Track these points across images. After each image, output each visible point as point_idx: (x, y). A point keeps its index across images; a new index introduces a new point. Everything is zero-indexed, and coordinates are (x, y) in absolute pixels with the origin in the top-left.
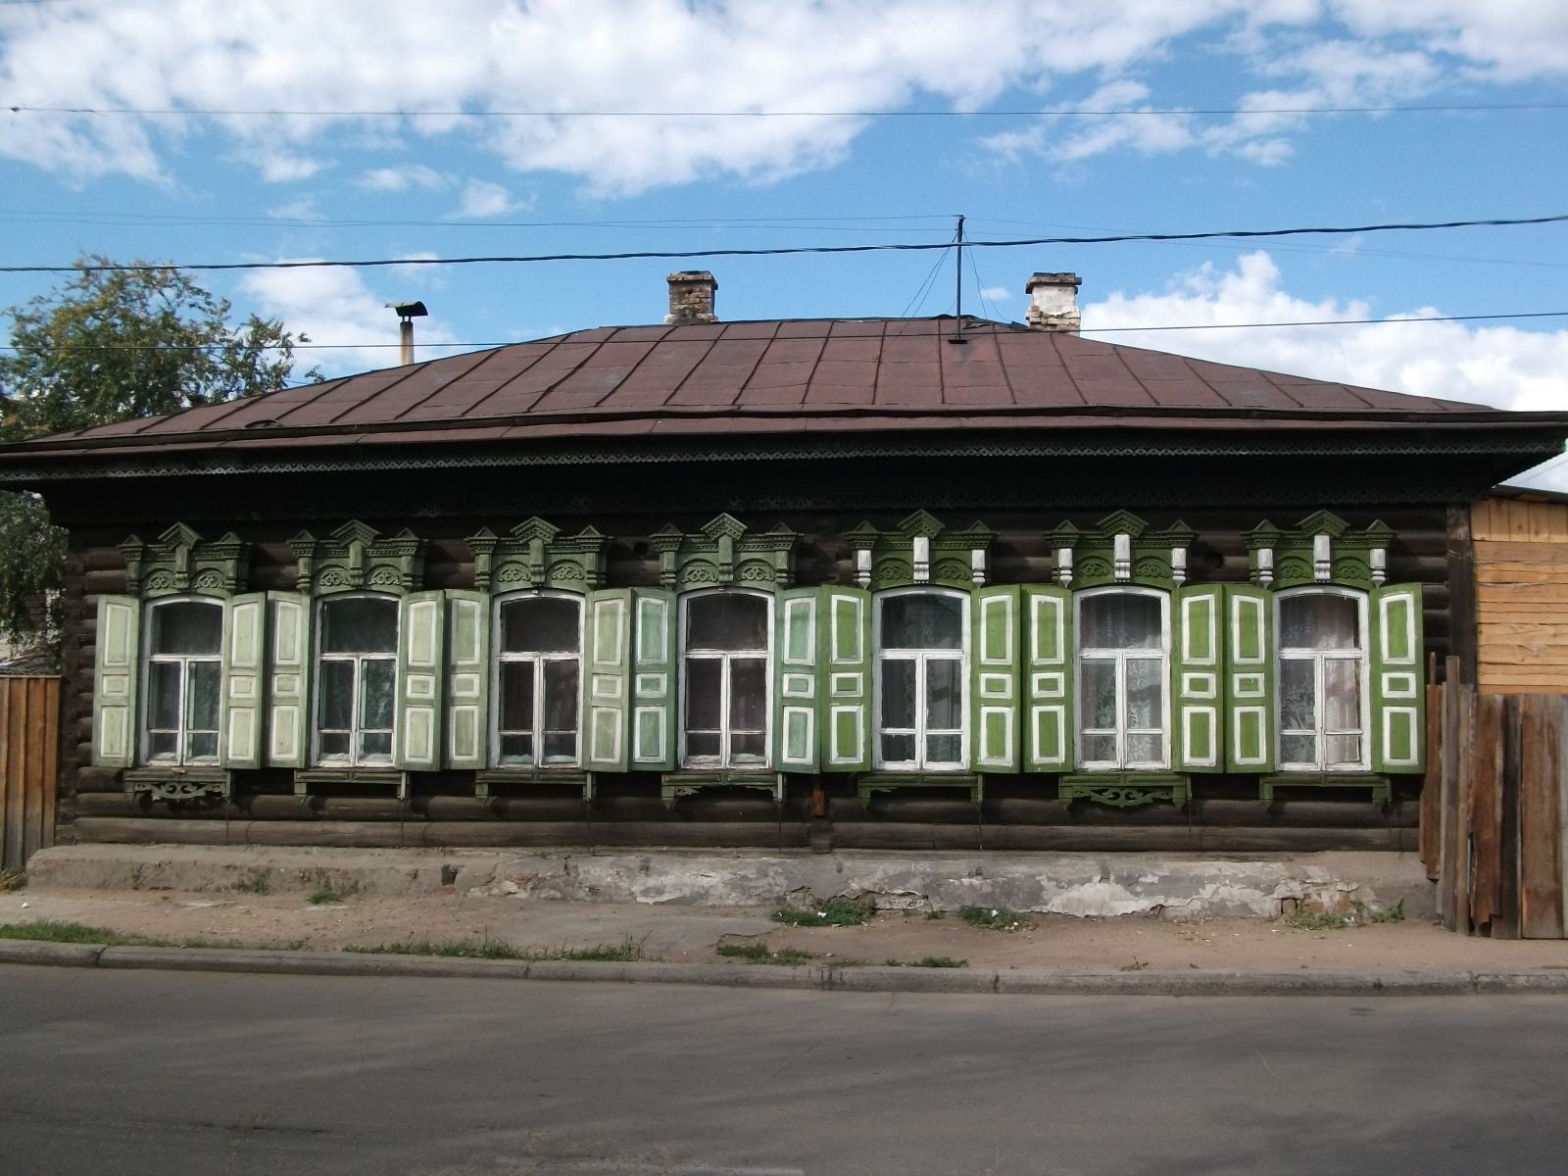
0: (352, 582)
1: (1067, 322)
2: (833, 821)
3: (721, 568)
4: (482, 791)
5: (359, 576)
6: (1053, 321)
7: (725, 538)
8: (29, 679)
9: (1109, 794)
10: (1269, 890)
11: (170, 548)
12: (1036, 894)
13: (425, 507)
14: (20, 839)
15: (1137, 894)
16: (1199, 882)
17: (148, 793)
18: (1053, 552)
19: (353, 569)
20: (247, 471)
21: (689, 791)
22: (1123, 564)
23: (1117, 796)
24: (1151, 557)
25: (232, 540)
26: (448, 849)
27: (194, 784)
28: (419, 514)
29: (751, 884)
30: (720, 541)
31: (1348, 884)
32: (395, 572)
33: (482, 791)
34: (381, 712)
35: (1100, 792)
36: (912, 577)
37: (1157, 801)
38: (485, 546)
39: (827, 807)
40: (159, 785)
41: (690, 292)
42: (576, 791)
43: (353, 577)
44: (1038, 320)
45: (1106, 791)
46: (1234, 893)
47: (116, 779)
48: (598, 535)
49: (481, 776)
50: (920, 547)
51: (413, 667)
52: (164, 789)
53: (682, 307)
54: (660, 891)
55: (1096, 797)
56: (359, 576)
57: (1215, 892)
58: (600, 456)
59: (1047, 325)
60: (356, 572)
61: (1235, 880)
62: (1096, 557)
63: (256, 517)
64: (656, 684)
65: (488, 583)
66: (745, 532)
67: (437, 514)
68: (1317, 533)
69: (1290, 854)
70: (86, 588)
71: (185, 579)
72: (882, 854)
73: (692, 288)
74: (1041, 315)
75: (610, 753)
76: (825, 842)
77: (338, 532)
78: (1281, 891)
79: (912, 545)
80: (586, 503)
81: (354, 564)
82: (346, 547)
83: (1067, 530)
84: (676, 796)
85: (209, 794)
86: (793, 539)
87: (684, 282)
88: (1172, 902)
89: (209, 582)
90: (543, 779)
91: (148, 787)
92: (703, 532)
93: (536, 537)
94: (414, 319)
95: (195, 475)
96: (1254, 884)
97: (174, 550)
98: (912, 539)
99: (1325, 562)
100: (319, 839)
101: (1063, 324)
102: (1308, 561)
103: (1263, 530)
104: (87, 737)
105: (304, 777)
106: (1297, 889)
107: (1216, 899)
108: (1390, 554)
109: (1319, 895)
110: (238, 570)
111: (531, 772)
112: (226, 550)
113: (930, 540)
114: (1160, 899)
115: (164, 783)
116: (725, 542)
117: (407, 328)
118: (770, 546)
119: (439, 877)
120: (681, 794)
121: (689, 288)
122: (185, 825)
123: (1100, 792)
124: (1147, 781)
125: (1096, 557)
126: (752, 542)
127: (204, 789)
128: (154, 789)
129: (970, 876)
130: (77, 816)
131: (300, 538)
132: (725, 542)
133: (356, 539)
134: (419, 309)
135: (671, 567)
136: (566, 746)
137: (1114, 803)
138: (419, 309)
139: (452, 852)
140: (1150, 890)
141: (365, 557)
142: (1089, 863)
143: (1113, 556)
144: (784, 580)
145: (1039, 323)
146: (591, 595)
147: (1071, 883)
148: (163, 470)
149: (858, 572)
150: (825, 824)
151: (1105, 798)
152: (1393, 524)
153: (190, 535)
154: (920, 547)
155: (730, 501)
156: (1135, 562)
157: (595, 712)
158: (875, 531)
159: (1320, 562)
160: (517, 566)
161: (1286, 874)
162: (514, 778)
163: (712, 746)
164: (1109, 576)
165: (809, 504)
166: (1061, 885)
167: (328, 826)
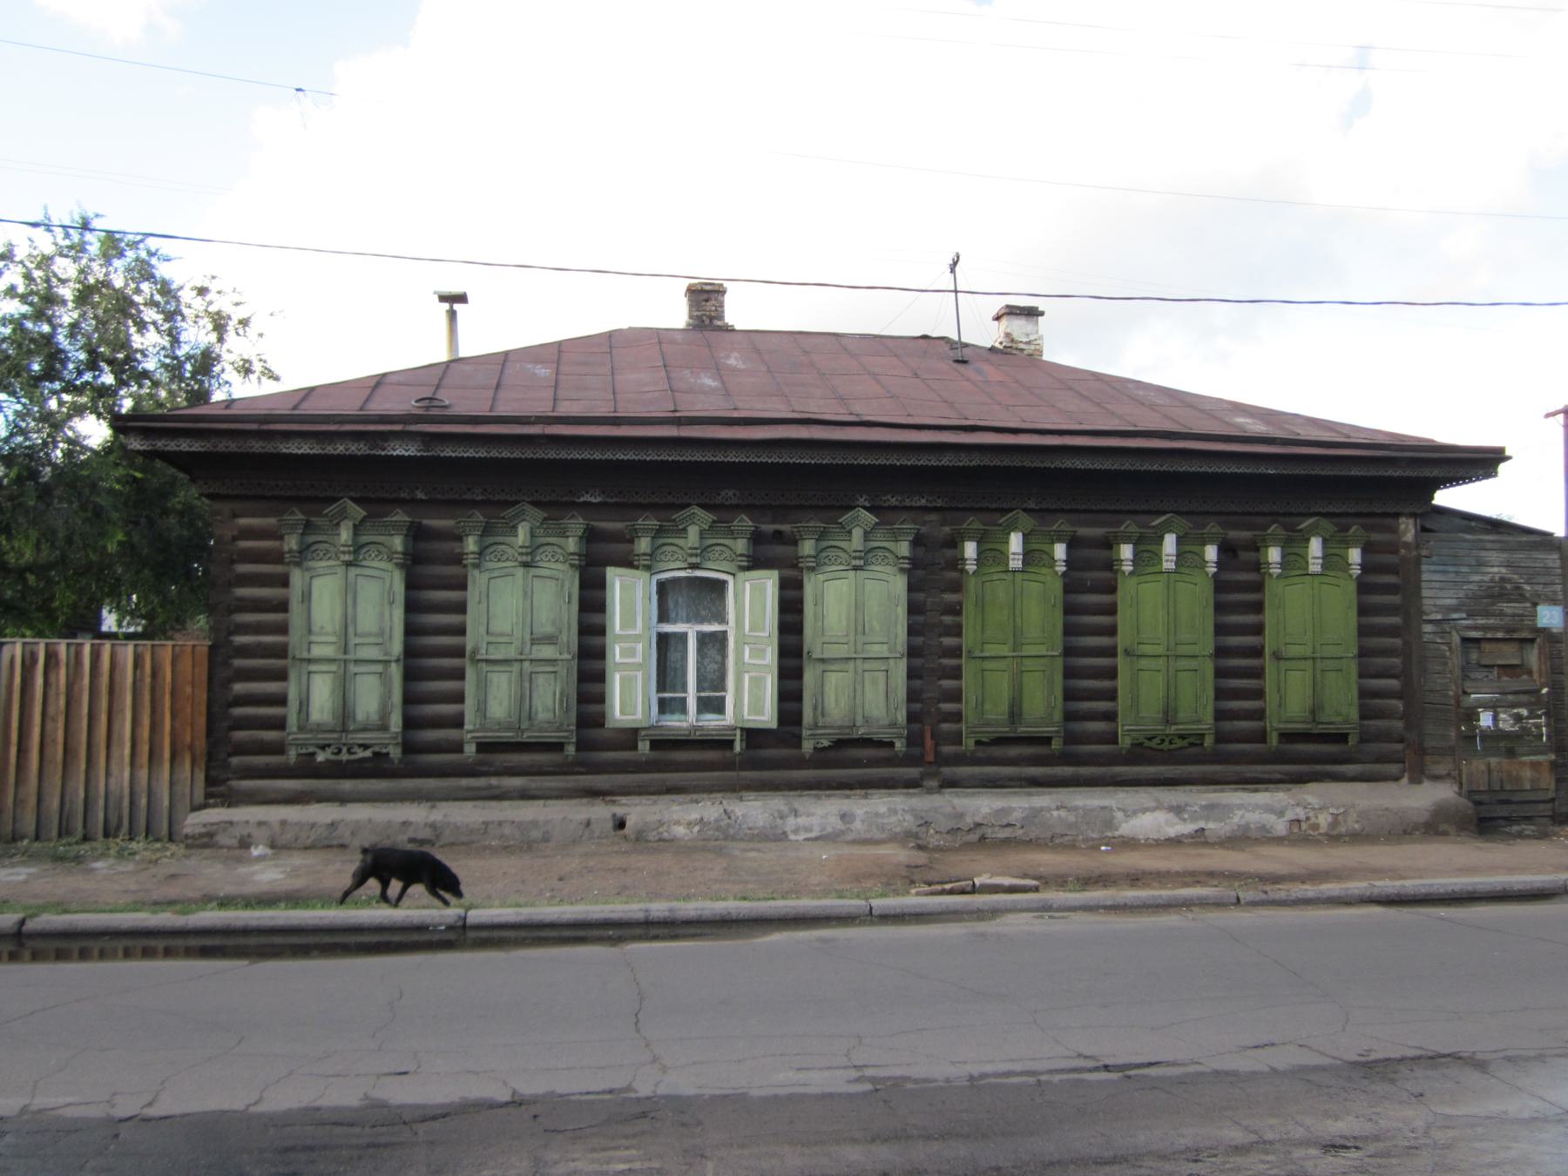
0: (520, 559)
1: (1033, 347)
2: (940, 766)
3: (690, 551)
4: (644, 747)
5: (527, 554)
6: (1021, 346)
7: (857, 529)
8: (194, 646)
9: (1157, 741)
10: (1281, 814)
11: (335, 522)
12: (1109, 824)
13: (587, 493)
14: (166, 803)
15: (1184, 820)
16: (1228, 809)
17: (313, 754)
18: (1115, 546)
19: (521, 547)
20: (430, 454)
21: (826, 743)
22: (1170, 558)
23: (1163, 741)
24: (548, 544)
25: (400, 517)
26: (608, 798)
27: (360, 746)
28: (582, 499)
29: (885, 821)
30: (853, 531)
31: (1338, 808)
32: (559, 551)
33: (644, 747)
34: (713, 681)
35: (1150, 739)
36: (1007, 564)
37: (1192, 745)
38: (647, 530)
39: (937, 753)
40: (323, 748)
41: (707, 301)
42: (729, 744)
43: (522, 554)
44: (1010, 345)
45: (1154, 738)
46: (1254, 818)
47: (630, 737)
48: (751, 524)
49: (643, 733)
50: (1015, 542)
51: (621, 636)
52: (329, 751)
53: (699, 313)
54: (808, 829)
55: (1147, 743)
56: (527, 554)
57: (1242, 817)
58: (709, 455)
59: (1017, 349)
60: (524, 550)
61: (1257, 807)
62: (1149, 551)
63: (420, 495)
64: (632, 653)
65: (477, 561)
66: (877, 524)
67: (598, 500)
68: (1313, 535)
69: (1289, 786)
70: (235, 557)
71: (349, 552)
72: (978, 793)
73: (705, 298)
74: (1012, 341)
75: (760, 712)
76: (934, 783)
77: (331, 509)
78: (1290, 815)
79: (1008, 538)
80: (735, 495)
81: (523, 542)
82: (515, 527)
83: (1131, 529)
84: (815, 748)
85: (376, 754)
86: (408, 524)
87: (702, 291)
88: (1211, 825)
89: (373, 555)
90: (700, 735)
91: (311, 750)
92: (841, 523)
93: (694, 523)
94: (456, 307)
95: (374, 455)
96: (1269, 809)
97: (338, 524)
98: (1009, 534)
99: (1317, 558)
100: (484, 793)
101: (1029, 349)
102: (1304, 558)
103: (1127, 530)
104: (601, 699)
105: (474, 737)
106: (1300, 813)
107: (1243, 822)
108: (1365, 551)
109: (1317, 817)
110: (405, 544)
111: (687, 729)
112: (396, 527)
113: (1024, 535)
114: (1202, 824)
115: (329, 746)
116: (857, 533)
117: (452, 315)
118: (732, 534)
119: (610, 825)
120: (819, 746)
121: (705, 296)
122: (347, 785)
123: (1150, 739)
124: (488, 737)
125: (1149, 551)
126: (880, 533)
127: (1186, 741)
128: (319, 751)
129: (1058, 808)
130: (228, 779)
131: (469, 517)
132: (857, 533)
133: (524, 520)
134: (462, 298)
135: (813, 553)
136: (717, 706)
137: (1160, 747)
138: (462, 298)
139: (614, 802)
140: (1194, 819)
141: (533, 536)
142: (1144, 796)
143: (1161, 550)
144: (906, 566)
145: (1010, 347)
146: (741, 575)
147: (1135, 813)
148: (494, 451)
149: (1350, 565)
150: (933, 769)
151: (1154, 744)
152: (1365, 527)
153: (359, 512)
154: (1015, 542)
155: (864, 497)
156: (1180, 555)
157: (747, 677)
158: (913, 526)
159: (1014, 554)
160: (674, 548)
161: (1292, 802)
162: (673, 735)
163: (681, 706)
164: (1159, 567)
165: (923, 502)
166: (1130, 814)
167: (494, 781)
